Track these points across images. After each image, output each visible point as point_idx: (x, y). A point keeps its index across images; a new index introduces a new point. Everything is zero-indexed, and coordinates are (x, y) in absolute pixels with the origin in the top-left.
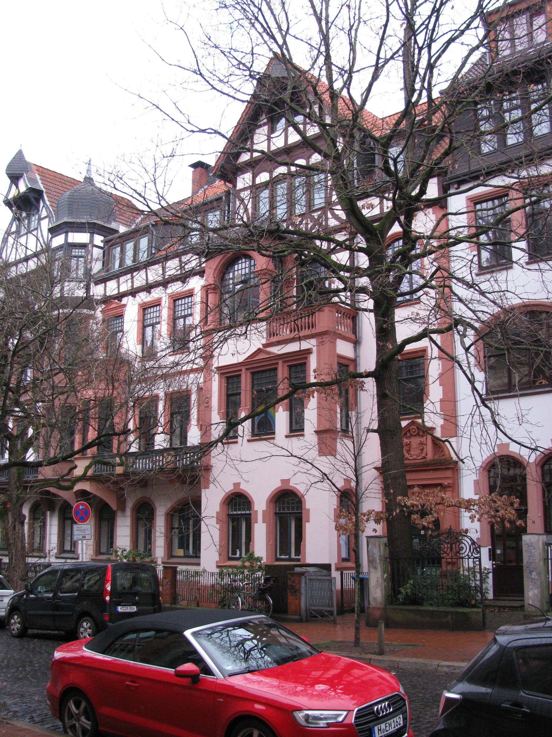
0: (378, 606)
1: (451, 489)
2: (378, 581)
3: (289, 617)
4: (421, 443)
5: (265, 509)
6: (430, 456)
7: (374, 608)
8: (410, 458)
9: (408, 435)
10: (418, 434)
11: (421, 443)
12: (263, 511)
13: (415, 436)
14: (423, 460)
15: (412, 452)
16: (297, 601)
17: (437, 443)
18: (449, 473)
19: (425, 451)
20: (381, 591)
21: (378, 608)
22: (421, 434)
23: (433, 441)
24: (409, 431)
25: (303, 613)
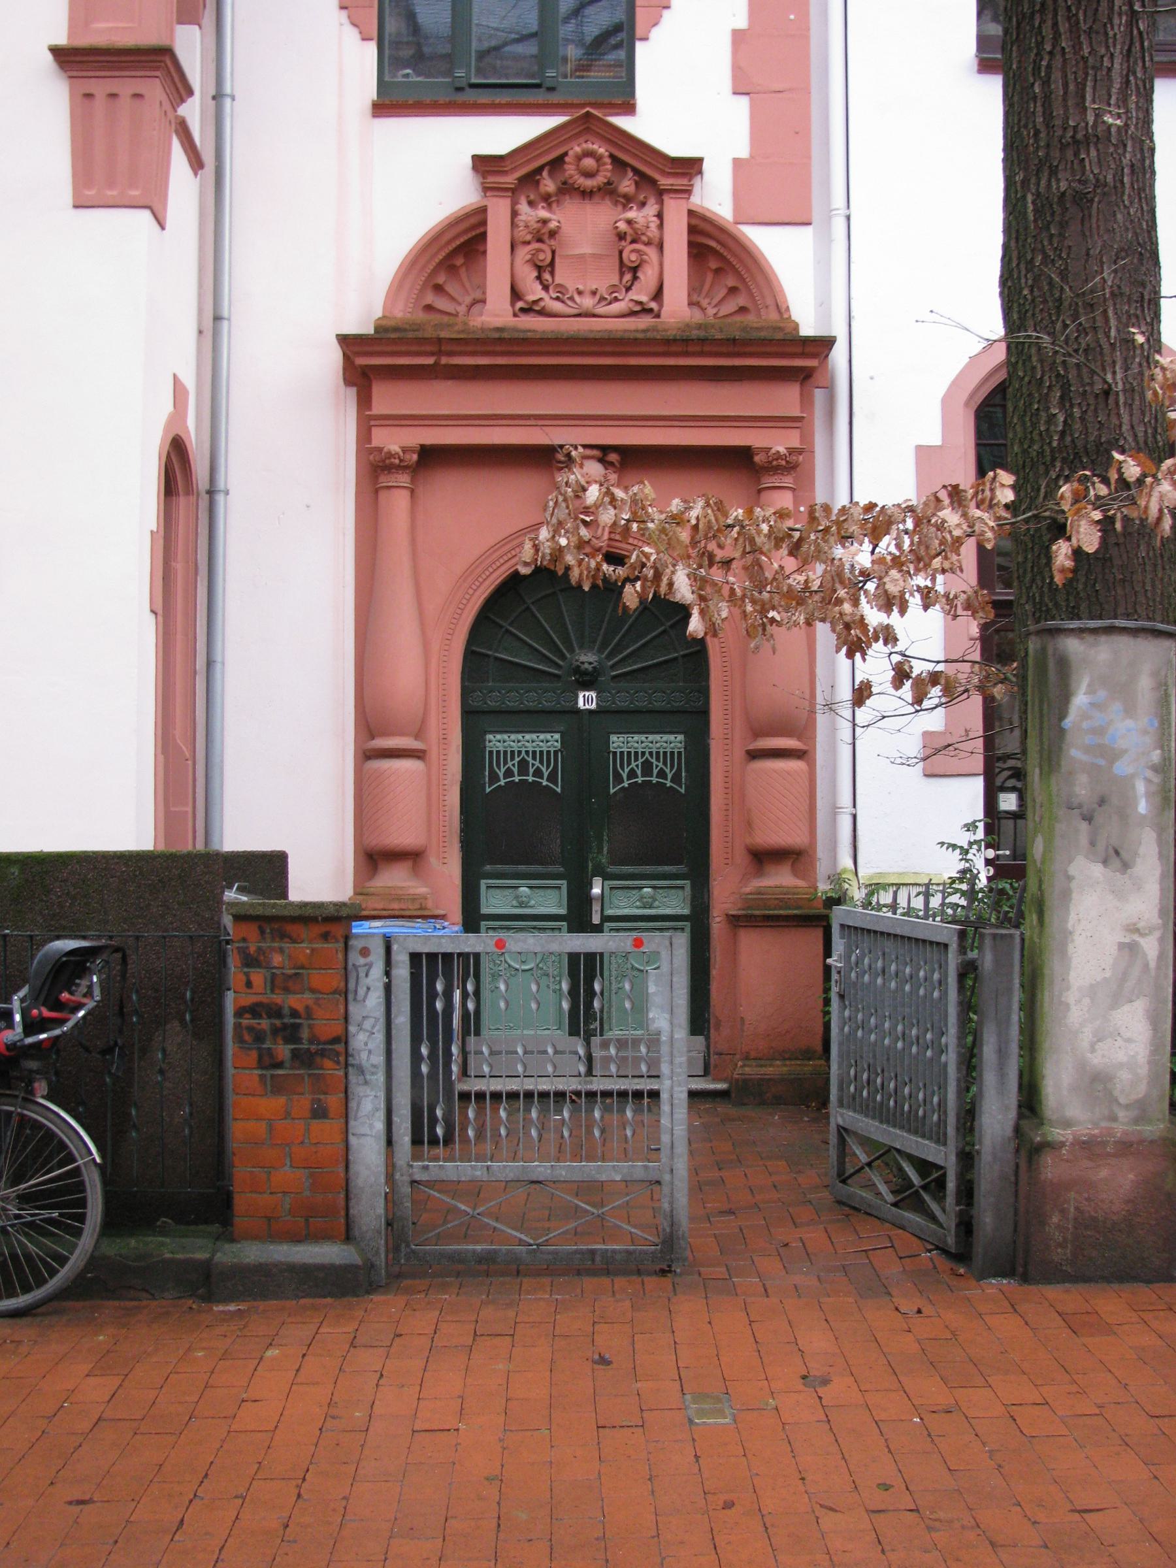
0: (1123, 1125)
1: (788, 481)
2: (1130, 949)
3: (252, 1253)
4: (628, 236)
5: (744, 152)
6: (677, 307)
7: (1089, 1147)
8: (557, 306)
9: (549, 185)
10: (608, 191)
11: (628, 236)
12: (737, 163)
13: (587, 194)
14: (644, 322)
15: (564, 276)
16: (326, 1129)
17: (715, 251)
18: (783, 399)
19: (648, 276)
20: (1154, 1020)
21: (1126, 1148)
22: (627, 185)
23: (692, 230)
24: (557, 163)
25: (370, 1211)
